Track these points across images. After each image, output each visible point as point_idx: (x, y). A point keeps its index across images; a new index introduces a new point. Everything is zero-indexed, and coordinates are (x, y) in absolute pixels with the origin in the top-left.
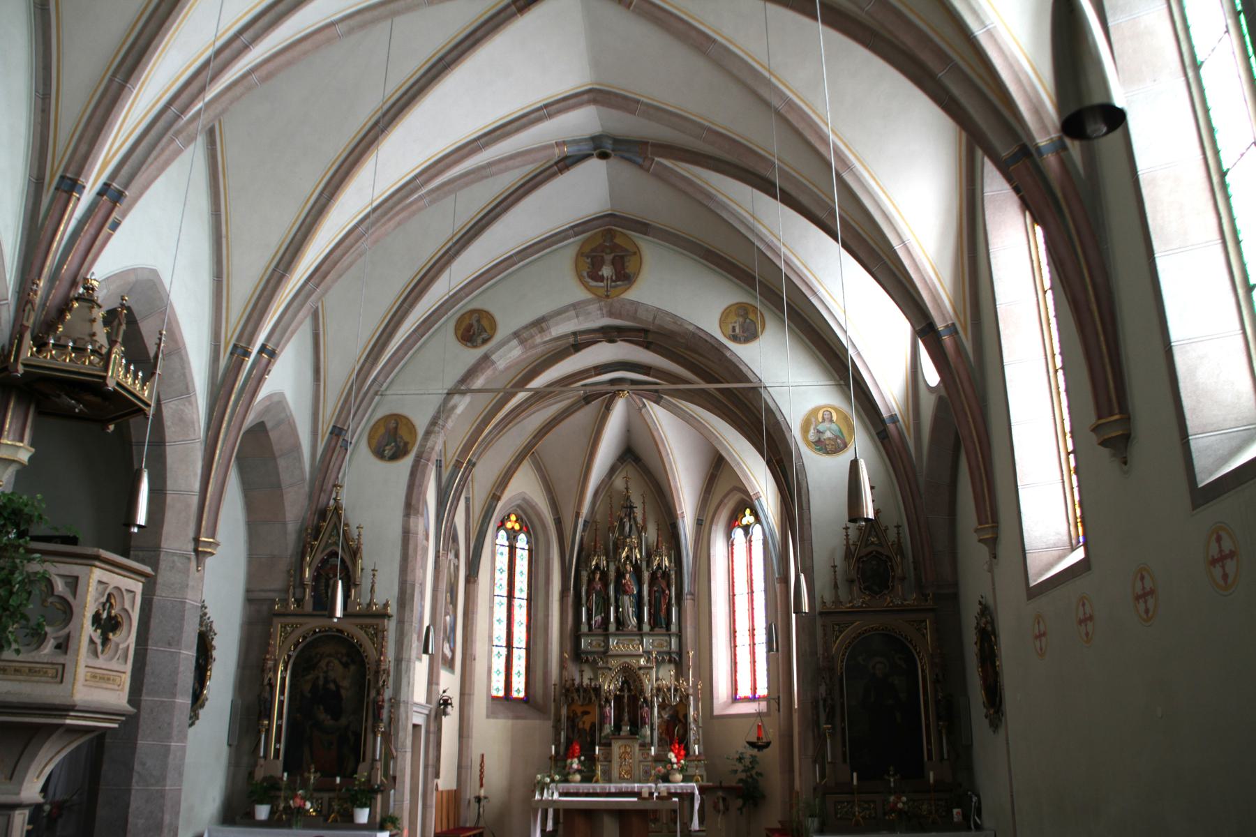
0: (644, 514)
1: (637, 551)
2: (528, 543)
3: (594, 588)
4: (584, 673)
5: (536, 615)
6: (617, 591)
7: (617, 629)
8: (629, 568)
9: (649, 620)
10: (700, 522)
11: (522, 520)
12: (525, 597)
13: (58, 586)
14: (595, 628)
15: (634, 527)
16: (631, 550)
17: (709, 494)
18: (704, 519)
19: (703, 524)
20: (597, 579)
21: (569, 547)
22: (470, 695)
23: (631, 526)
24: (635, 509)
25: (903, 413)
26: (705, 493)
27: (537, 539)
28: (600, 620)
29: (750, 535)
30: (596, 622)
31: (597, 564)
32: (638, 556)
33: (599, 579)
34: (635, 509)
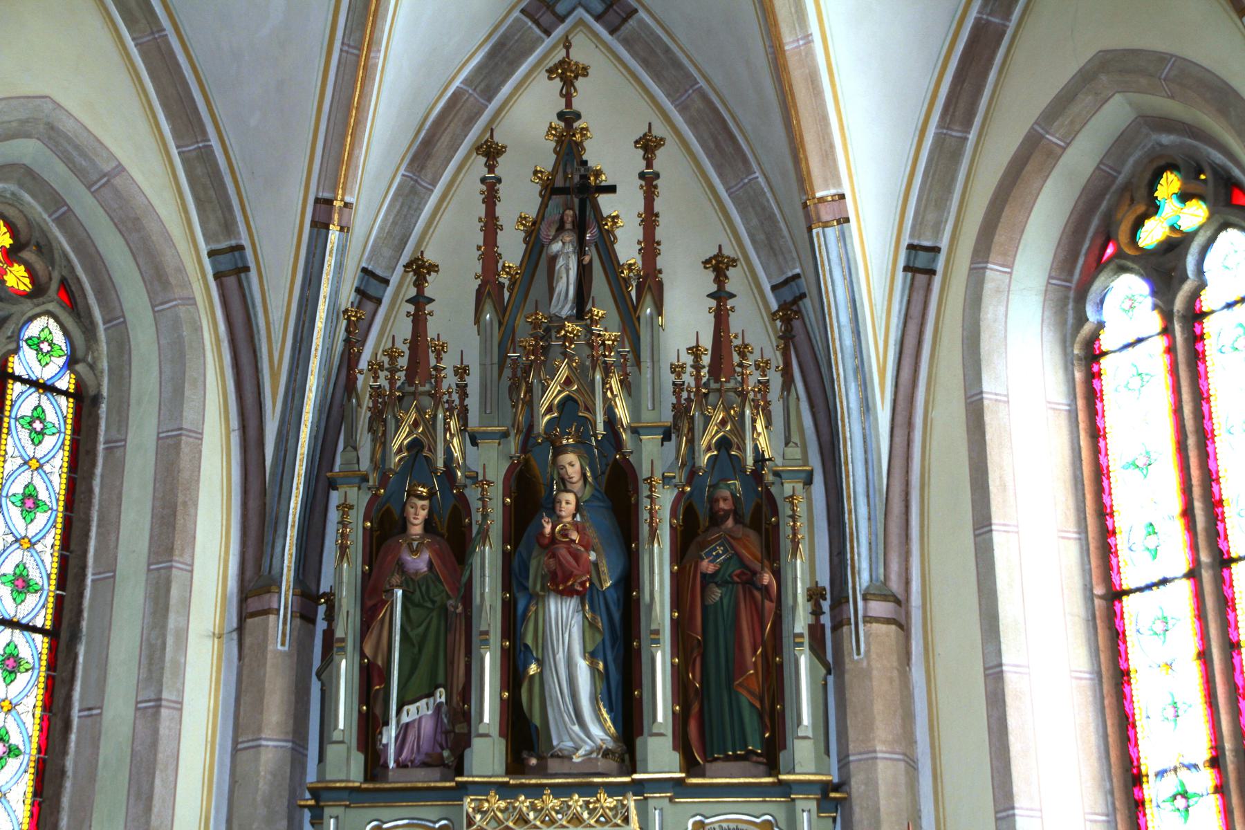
0: (649, 219)
1: (614, 383)
2: (71, 363)
3: (401, 567)
4: (580, 83)
5: (94, 710)
6: (512, 576)
7: (515, 765)
8: (572, 464)
9: (680, 721)
10: (922, 260)
11: (45, 248)
12: (43, 619)
13: (1113, 725)
14: (400, 765)
15: (600, 285)
16: (580, 375)
17: (968, 124)
18: (944, 244)
19: (940, 266)
20: (416, 529)
21: (279, 349)
22: (1055, 313)
23: (584, 273)
24: (604, 200)
25: (1063, 277)
26: (943, 123)
27: (89, 330)
28: (427, 727)
29: (1187, 287)
30: (404, 730)
31: (415, 446)
32: (622, 412)
33: (428, 525)
34: (604, 200)
